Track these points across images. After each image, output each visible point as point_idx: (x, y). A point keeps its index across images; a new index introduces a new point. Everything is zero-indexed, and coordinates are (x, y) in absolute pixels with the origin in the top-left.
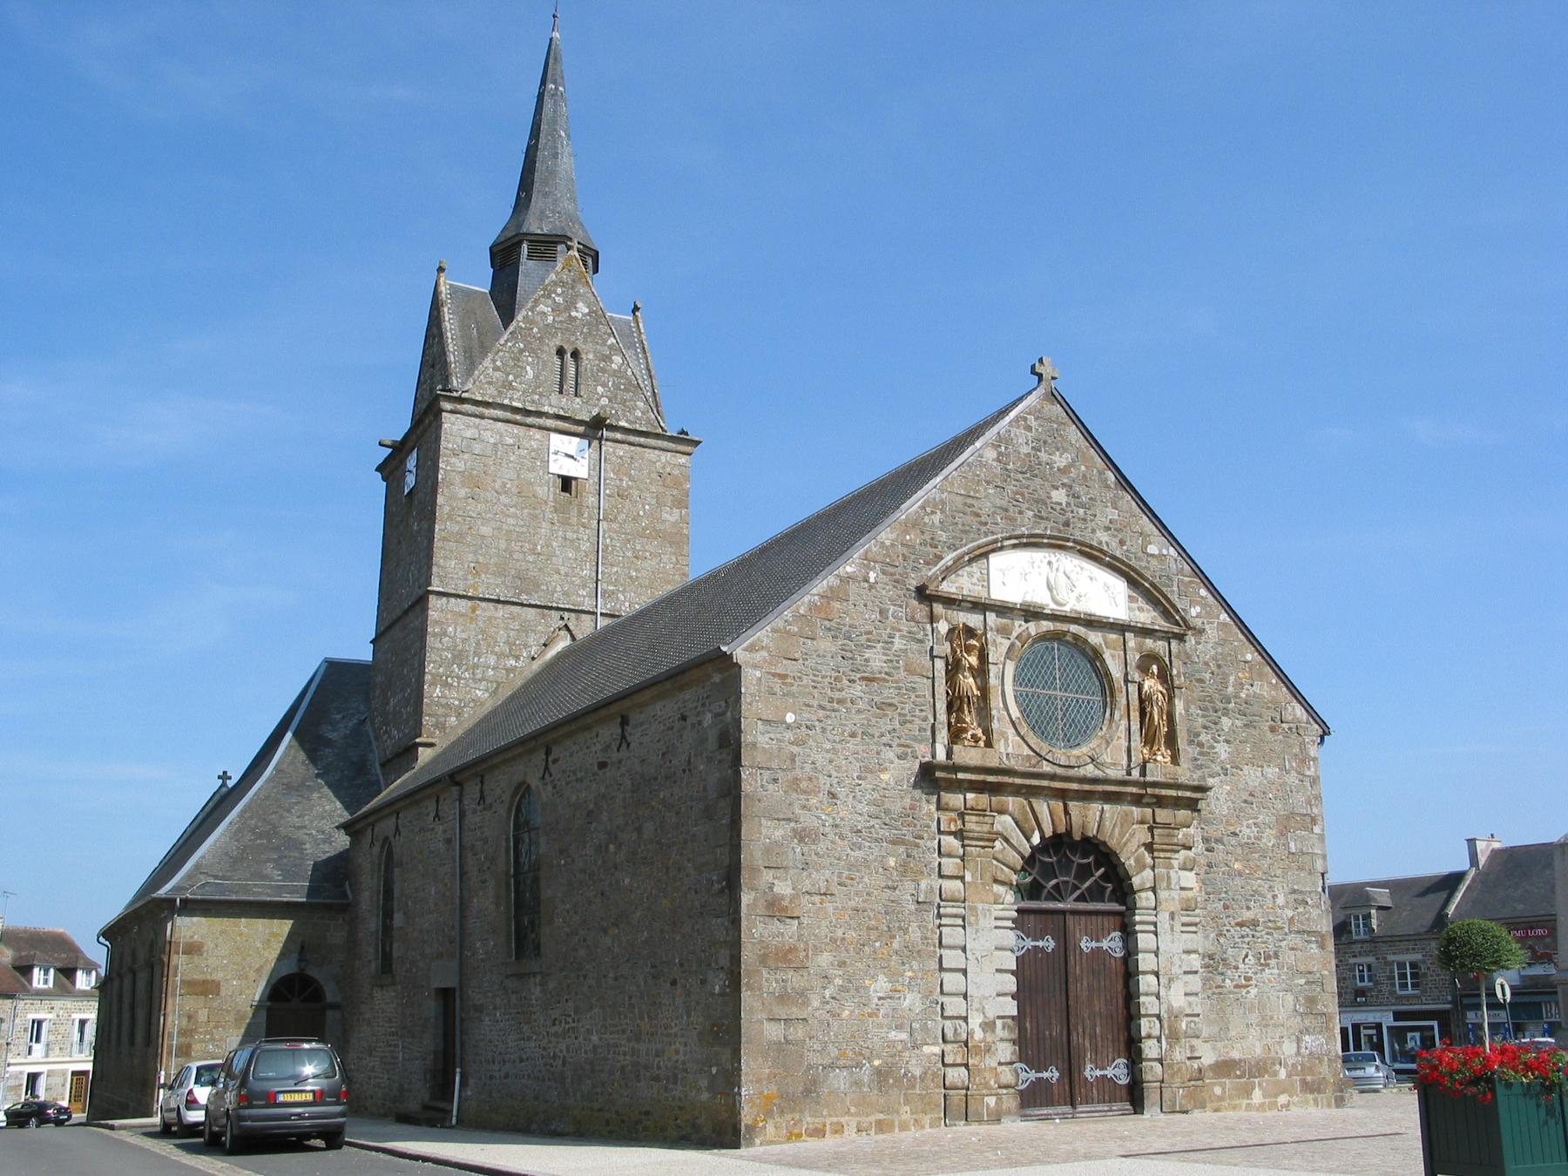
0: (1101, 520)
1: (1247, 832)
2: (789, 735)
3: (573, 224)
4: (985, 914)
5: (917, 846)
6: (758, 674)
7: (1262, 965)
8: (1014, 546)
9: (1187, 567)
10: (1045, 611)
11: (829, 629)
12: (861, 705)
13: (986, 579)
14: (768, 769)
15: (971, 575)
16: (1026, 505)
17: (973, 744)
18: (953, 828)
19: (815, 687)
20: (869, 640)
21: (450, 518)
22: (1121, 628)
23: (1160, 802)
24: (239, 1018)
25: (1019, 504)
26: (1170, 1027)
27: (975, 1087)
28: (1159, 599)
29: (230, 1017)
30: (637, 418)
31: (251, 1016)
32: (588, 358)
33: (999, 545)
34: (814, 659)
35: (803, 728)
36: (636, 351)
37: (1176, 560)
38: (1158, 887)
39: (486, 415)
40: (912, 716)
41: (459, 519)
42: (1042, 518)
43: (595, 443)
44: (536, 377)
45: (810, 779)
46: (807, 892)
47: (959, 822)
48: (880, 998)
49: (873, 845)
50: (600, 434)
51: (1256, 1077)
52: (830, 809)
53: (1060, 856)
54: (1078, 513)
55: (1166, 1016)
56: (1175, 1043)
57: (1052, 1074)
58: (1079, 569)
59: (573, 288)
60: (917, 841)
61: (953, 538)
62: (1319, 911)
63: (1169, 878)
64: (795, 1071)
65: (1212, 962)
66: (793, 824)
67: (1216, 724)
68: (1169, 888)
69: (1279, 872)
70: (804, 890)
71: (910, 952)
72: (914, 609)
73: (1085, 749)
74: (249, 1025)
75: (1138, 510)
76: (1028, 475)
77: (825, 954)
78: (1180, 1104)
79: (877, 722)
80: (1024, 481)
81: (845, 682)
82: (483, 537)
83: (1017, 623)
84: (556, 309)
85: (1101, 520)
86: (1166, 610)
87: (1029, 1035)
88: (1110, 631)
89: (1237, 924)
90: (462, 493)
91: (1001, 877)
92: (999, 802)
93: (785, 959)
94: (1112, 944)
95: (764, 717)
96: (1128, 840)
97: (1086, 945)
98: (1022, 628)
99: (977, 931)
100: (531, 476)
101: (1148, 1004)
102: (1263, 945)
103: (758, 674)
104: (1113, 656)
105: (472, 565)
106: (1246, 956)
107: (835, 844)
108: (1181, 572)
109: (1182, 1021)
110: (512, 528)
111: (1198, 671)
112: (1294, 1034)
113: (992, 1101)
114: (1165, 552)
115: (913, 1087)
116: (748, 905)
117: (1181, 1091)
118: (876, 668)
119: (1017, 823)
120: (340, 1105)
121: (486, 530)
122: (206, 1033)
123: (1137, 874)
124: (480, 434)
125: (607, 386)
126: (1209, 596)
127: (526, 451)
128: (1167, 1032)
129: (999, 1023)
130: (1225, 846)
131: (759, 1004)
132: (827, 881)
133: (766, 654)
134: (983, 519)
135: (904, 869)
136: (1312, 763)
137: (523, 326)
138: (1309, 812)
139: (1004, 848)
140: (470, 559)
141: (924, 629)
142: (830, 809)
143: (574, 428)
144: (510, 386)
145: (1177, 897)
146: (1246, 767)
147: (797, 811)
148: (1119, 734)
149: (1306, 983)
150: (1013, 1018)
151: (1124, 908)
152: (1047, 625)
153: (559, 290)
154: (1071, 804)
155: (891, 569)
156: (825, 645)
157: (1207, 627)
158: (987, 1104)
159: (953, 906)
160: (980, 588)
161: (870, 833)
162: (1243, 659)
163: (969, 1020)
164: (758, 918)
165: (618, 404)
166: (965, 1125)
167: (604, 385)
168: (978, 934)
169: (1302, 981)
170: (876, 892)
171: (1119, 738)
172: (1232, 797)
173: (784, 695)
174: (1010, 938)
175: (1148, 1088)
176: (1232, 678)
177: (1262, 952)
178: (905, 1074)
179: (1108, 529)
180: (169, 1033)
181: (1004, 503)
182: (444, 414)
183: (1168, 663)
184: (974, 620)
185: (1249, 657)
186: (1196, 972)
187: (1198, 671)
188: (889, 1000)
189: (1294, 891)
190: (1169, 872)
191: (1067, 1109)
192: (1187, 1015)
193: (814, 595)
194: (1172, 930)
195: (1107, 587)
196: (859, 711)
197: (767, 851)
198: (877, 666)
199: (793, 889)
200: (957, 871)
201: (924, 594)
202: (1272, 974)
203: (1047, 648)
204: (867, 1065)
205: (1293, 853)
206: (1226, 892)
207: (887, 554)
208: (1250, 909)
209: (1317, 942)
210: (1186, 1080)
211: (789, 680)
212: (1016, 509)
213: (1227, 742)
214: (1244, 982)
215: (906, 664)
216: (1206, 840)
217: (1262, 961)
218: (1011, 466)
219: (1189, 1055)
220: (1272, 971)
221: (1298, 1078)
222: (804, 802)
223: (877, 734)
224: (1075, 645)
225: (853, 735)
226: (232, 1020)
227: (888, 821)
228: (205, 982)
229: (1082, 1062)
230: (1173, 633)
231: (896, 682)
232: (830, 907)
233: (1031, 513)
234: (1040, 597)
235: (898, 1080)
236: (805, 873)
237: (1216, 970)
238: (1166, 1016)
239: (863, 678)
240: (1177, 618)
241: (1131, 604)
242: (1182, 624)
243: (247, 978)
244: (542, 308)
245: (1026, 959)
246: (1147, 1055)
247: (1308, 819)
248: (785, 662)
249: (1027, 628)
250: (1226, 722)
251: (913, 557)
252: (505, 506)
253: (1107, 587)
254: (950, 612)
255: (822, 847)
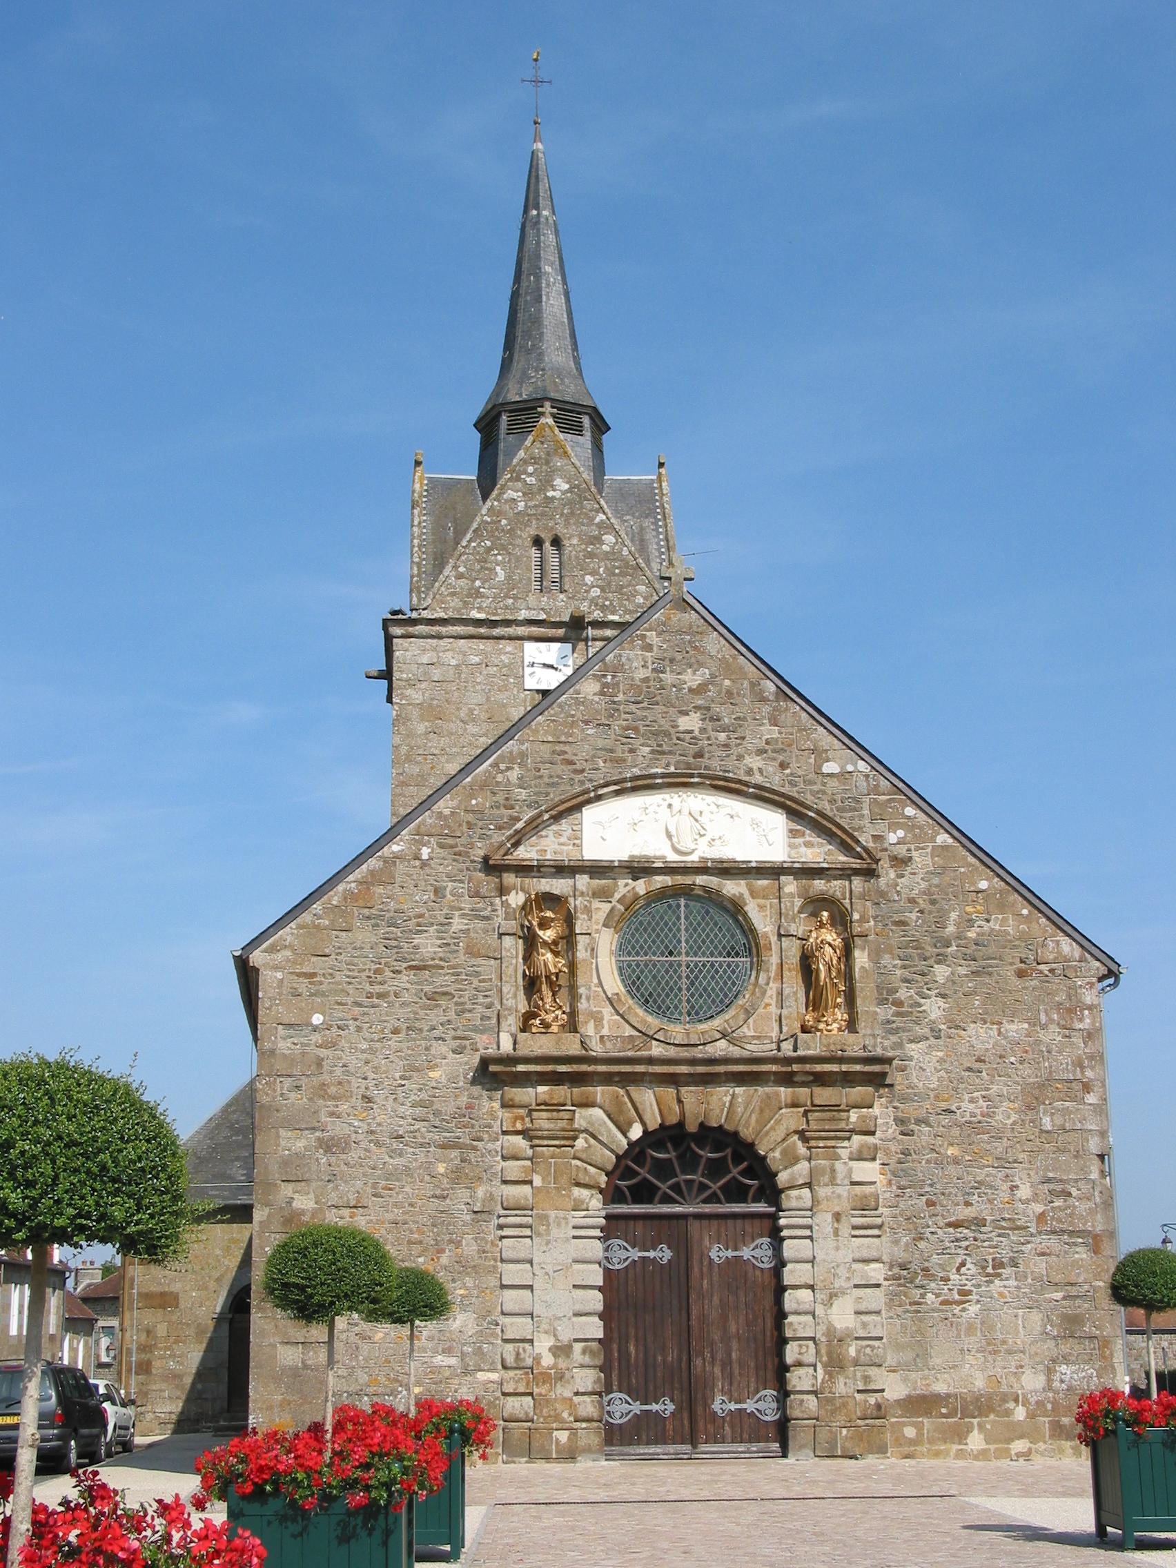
0: (753, 742)
1: (968, 1108)
2: (317, 1038)
3: (562, 380)
5: (475, 1149)
6: (279, 975)
7: (988, 1275)
8: (618, 793)
9: (884, 784)
10: (655, 865)
11: (369, 918)
12: (406, 997)
13: (576, 839)
15: (558, 834)
16: (642, 741)
17: (543, 1030)
18: (519, 1126)
19: (350, 983)
21: (533, 731)
22: (774, 871)
23: (821, 1080)
24: (200, 1331)
25: (629, 740)
26: (829, 1354)
27: (541, 1420)
28: (830, 829)
29: (191, 1332)
31: (211, 1329)
32: (572, 543)
33: (592, 794)
34: (349, 952)
35: (334, 1029)
36: (655, 518)
37: (867, 776)
38: (814, 1182)
39: (444, 634)
40: (474, 1004)
42: (663, 753)
43: (581, 645)
44: (509, 577)
45: (340, 1083)
47: (527, 1120)
50: (585, 635)
51: (974, 1417)
52: (365, 1114)
53: (682, 1149)
54: (717, 739)
55: (824, 1339)
56: (838, 1373)
57: (664, 1407)
58: (714, 808)
59: (547, 463)
60: (475, 1143)
63: (833, 1171)
64: (314, 1398)
65: (905, 1273)
66: (318, 1134)
67: (923, 975)
68: (833, 1182)
69: (1021, 1156)
70: (329, 1204)
72: (480, 882)
73: (717, 1022)
74: (211, 1339)
75: (811, 721)
76: (645, 704)
78: (842, 1448)
79: (427, 1014)
80: (639, 713)
81: (388, 974)
83: (621, 882)
84: (528, 493)
85: (753, 742)
86: (845, 841)
87: (633, 1360)
88: (759, 876)
89: (949, 1225)
90: (421, 728)
91: (583, 1179)
92: (582, 1094)
94: (757, 1253)
96: (772, 1128)
97: (718, 1253)
98: (628, 888)
99: (548, 1243)
100: (502, 697)
101: (796, 1324)
102: (991, 1250)
103: (279, 975)
104: (761, 907)
106: (963, 1264)
107: (369, 1152)
108: (876, 790)
109: (849, 1345)
111: (897, 912)
112: (1042, 1363)
113: (563, 1436)
114: (850, 768)
116: (261, 1222)
117: (844, 1431)
118: (428, 955)
119: (609, 1116)
120: (54, 1428)
122: (167, 1348)
123: (786, 1168)
124: (439, 657)
125: (598, 574)
127: (495, 669)
128: (825, 1359)
129: (578, 1347)
131: (272, 1326)
132: (358, 1192)
133: (289, 953)
134: (578, 767)
135: (457, 1176)
137: (489, 520)
138: (1079, 1076)
139: (590, 1146)
141: (492, 904)
142: (365, 1114)
143: (551, 632)
144: (478, 594)
145: (845, 1194)
146: (972, 1025)
147: (323, 1119)
148: (767, 1000)
149: (1064, 1298)
150: (600, 1340)
151: (774, 1209)
152: (660, 881)
153: (530, 469)
154: (683, 1090)
155: (450, 841)
156: (364, 935)
157: (914, 854)
158: (557, 1439)
159: (516, 1215)
160: (571, 847)
161: (415, 1137)
162: (972, 889)
163: (535, 1344)
164: (273, 1235)
165: (613, 592)
166: (527, 1462)
167: (594, 573)
168: (550, 1246)
169: (1059, 1295)
171: (768, 1005)
172: (947, 1066)
173: (312, 995)
174: (596, 1249)
175: (795, 1426)
176: (953, 916)
177: (990, 1258)
179: (761, 752)
180: (128, 1349)
181: (609, 743)
182: (395, 640)
183: (849, 907)
184: (558, 886)
185: (983, 885)
186: (878, 1286)
187: (897, 912)
189: (1048, 1180)
190: (833, 1165)
191: (687, 1448)
192: (857, 1338)
193: (350, 883)
194: (836, 1233)
195: (755, 824)
196: (404, 1004)
197: (285, 1163)
198: (428, 952)
199: (316, 1203)
200: (523, 1175)
201: (491, 867)
202: (1005, 1287)
203: (670, 906)
204: (405, 1392)
205: (1048, 1132)
206: (931, 1185)
207: (445, 825)
208: (971, 1204)
210: (854, 1417)
212: (626, 748)
213: (943, 996)
214: (957, 1297)
215: (468, 946)
216: (900, 1121)
217: (990, 1270)
218: (621, 697)
220: (1005, 1283)
221: (1047, 1419)
222: (332, 1109)
224: (710, 899)
225: (396, 1031)
226: (193, 1334)
227: (437, 1123)
228: (163, 1294)
229: (708, 1392)
231: (453, 967)
234: (658, 848)
236: (331, 1185)
237: (911, 1282)
240: (859, 849)
241: (793, 840)
242: (864, 855)
243: (206, 1288)
244: (511, 494)
245: (631, 1272)
247: (1077, 1086)
248: (314, 959)
249: (633, 888)
250: (941, 972)
251: (480, 823)
252: (473, 735)
253: (755, 824)
254: (527, 880)
255: (353, 1155)
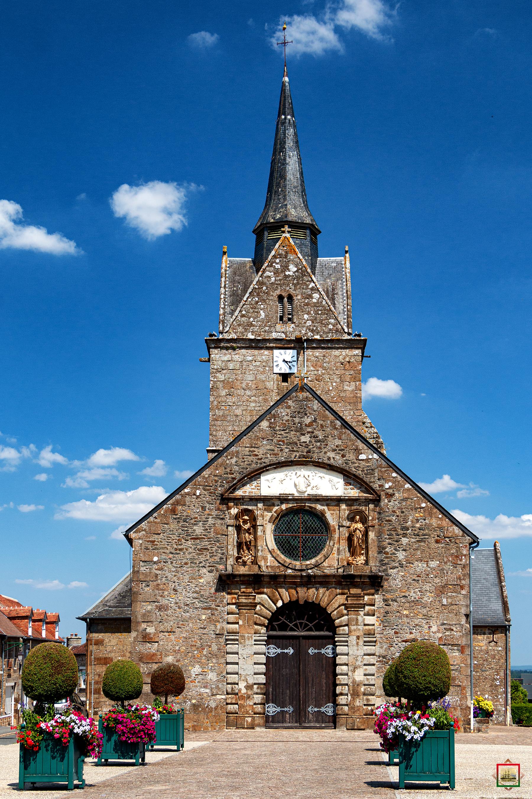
1: (413, 595)
2: (155, 566)
4: (249, 639)
5: (217, 610)
6: (141, 542)
9: (384, 463)
11: (175, 519)
12: (190, 550)
14: (145, 581)
20: (195, 521)
22: (337, 501)
30: (330, 330)
32: (298, 298)
40: (217, 553)
41: (223, 407)
46: (162, 631)
48: (196, 675)
49: (194, 611)
55: (351, 684)
56: (357, 698)
59: (286, 257)
61: (242, 469)
62: (461, 634)
63: (357, 619)
66: (156, 603)
67: (397, 541)
68: (357, 624)
69: (435, 615)
71: (212, 655)
73: (313, 561)
76: (287, 431)
77: (170, 656)
78: (357, 726)
80: (285, 435)
82: (237, 416)
84: (276, 272)
89: (403, 641)
90: (223, 393)
93: (151, 659)
95: (143, 560)
97: (311, 651)
100: (263, 377)
101: (341, 679)
103: (141, 542)
105: (231, 432)
110: (253, 409)
113: (249, 720)
114: (370, 457)
115: (211, 712)
117: (358, 720)
119: (269, 597)
121: (238, 412)
125: (310, 314)
126: (398, 476)
127: (259, 363)
128: (351, 692)
129: (255, 687)
130: (398, 602)
134: (260, 457)
136: (463, 557)
137: (257, 287)
140: (230, 429)
145: (361, 629)
150: (264, 684)
156: (173, 525)
158: (247, 721)
159: (232, 636)
161: (193, 605)
167: (309, 313)
170: (195, 630)
176: (411, 518)
178: (207, 707)
179: (334, 450)
185: (423, 505)
186: (374, 665)
188: (201, 676)
192: (365, 685)
196: (190, 553)
197: (144, 615)
204: (189, 702)
205: (444, 605)
208: (412, 633)
209: (458, 650)
210: (362, 714)
211: (156, 543)
219: (365, 703)
223: (198, 562)
228: (105, 658)
230: (369, 499)
232: (172, 637)
233: (288, 450)
235: (204, 709)
238: (351, 684)
239: (192, 539)
244: (267, 273)
246: (339, 702)
250: (405, 541)
